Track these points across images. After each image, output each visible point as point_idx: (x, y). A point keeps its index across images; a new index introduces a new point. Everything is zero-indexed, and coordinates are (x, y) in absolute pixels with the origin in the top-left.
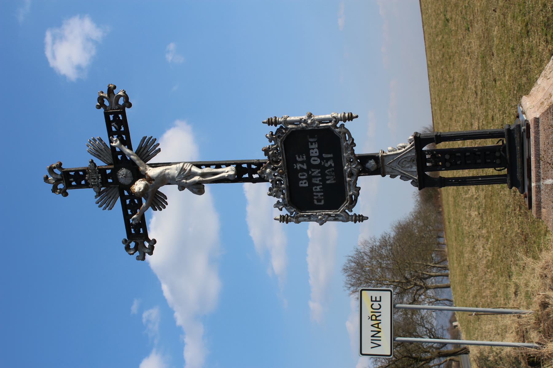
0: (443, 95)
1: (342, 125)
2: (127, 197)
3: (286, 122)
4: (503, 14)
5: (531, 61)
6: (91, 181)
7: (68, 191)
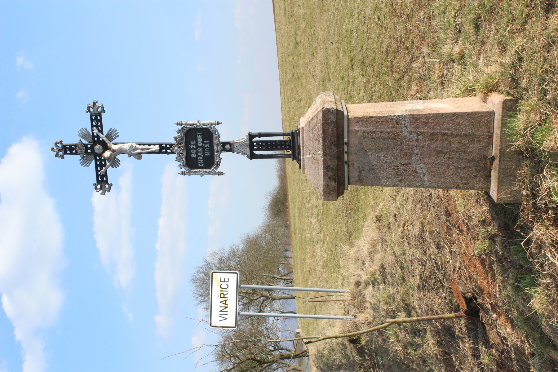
0: (292, 112)
1: (214, 127)
2: (98, 160)
3: (187, 124)
4: (337, 47)
5: (354, 89)
6: (79, 151)
7: (64, 156)
